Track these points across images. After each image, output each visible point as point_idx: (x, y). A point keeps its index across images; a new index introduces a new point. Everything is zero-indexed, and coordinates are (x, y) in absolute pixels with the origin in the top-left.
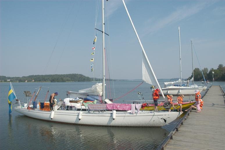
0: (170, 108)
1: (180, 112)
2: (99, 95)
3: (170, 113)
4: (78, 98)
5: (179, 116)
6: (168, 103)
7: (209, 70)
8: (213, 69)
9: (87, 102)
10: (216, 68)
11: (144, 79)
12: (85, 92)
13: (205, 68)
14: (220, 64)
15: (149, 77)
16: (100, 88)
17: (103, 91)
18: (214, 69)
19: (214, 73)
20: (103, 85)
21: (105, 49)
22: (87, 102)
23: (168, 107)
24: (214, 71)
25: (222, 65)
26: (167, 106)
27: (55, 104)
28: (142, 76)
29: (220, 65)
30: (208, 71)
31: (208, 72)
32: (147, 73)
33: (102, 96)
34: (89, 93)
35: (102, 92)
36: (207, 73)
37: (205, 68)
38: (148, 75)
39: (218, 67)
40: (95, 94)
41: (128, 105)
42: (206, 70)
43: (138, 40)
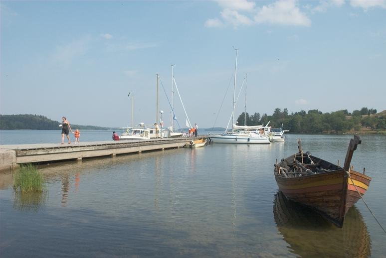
8: (266, 114)
13: (256, 113)
29: (276, 109)
37: (256, 113)
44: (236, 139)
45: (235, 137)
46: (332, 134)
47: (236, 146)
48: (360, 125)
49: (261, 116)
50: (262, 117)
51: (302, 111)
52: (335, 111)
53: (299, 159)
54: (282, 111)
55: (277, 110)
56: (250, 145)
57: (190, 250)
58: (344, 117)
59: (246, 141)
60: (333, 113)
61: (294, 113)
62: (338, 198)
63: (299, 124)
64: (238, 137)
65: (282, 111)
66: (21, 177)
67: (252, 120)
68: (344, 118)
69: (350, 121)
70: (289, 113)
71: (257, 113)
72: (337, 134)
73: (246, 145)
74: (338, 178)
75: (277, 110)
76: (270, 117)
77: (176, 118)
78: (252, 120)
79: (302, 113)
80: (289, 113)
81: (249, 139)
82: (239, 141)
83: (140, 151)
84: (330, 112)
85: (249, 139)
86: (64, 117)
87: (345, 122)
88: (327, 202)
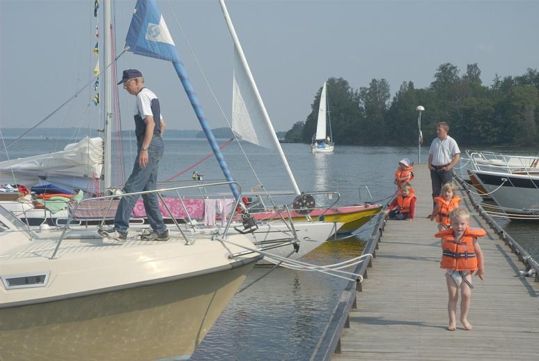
0: (311, 211)
1: (335, 222)
2: (90, 176)
3: (311, 224)
4: (9, 186)
5: (334, 232)
6: (305, 198)
7: (394, 91)
8: (411, 84)
9: (52, 198)
10: (424, 81)
11: (236, 128)
12: (35, 166)
13: (374, 81)
14: (445, 62)
15: (251, 125)
16: (97, 154)
17: (103, 163)
18: (417, 87)
19: (422, 108)
20: (103, 143)
21: (111, 28)
22: (52, 198)
23: (306, 208)
24: (421, 96)
25: (454, 68)
26: (303, 205)
27: (534, 111)
28: (231, 120)
29: (443, 68)
30: (389, 96)
31: (389, 102)
32: (247, 111)
33: (103, 177)
34: (49, 169)
35: (101, 166)
36: (385, 106)
37: (374, 81)
38: (249, 119)
39: (436, 76)
40: (80, 172)
41: (195, 203)
42: (378, 88)
43: (224, 12)
50: (400, 94)
54: (462, 72)
55: (446, 72)
61: (501, 79)
65: (462, 72)
66: (515, 104)
67: (362, 105)
70: (487, 81)
71: (379, 78)
74: (212, 239)
75: (446, 72)
76: (420, 93)
77: (164, 33)
78: (362, 105)
80: (487, 81)
83: (103, 220)
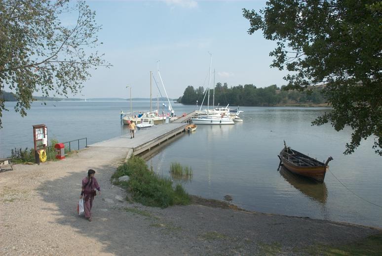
29: (218, 84)
44: (212, 121)
45: (211, 120)
46: (265, 106)
47: (212, 127)
48: (287, 98)
49: (205, 90)
51: (240, 86)
52: (267, 87)
53: (286, 151)
54: (223, 85)
56: (222, 126)
57: (43, 29)
58: (275, 92)
59: (219, 123)
60: (266, 88)
61: (233, 87)
62: (322, 174)
63: (238, 97)
64: (213, 120)
65: (223, 85)
68: (274, 93)
69: (279, 95)
70: (229, 87)
72: (269, 106)
73: (219, 126)
78: (197, 93)
79: (240, 88)
80: (229, 87)
81: (221, 121)
82: (213, 123)
84: (263, 87)
85: (221, 121)
86: (88, 219)
87: (276, 96)
88: (317, 176)
